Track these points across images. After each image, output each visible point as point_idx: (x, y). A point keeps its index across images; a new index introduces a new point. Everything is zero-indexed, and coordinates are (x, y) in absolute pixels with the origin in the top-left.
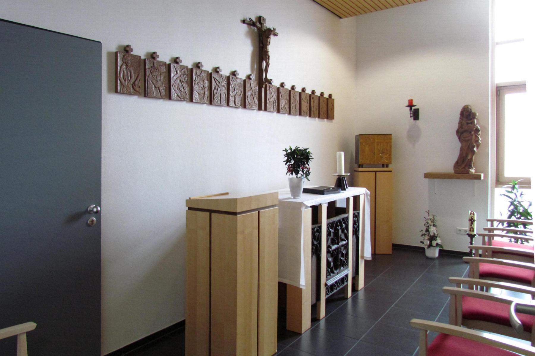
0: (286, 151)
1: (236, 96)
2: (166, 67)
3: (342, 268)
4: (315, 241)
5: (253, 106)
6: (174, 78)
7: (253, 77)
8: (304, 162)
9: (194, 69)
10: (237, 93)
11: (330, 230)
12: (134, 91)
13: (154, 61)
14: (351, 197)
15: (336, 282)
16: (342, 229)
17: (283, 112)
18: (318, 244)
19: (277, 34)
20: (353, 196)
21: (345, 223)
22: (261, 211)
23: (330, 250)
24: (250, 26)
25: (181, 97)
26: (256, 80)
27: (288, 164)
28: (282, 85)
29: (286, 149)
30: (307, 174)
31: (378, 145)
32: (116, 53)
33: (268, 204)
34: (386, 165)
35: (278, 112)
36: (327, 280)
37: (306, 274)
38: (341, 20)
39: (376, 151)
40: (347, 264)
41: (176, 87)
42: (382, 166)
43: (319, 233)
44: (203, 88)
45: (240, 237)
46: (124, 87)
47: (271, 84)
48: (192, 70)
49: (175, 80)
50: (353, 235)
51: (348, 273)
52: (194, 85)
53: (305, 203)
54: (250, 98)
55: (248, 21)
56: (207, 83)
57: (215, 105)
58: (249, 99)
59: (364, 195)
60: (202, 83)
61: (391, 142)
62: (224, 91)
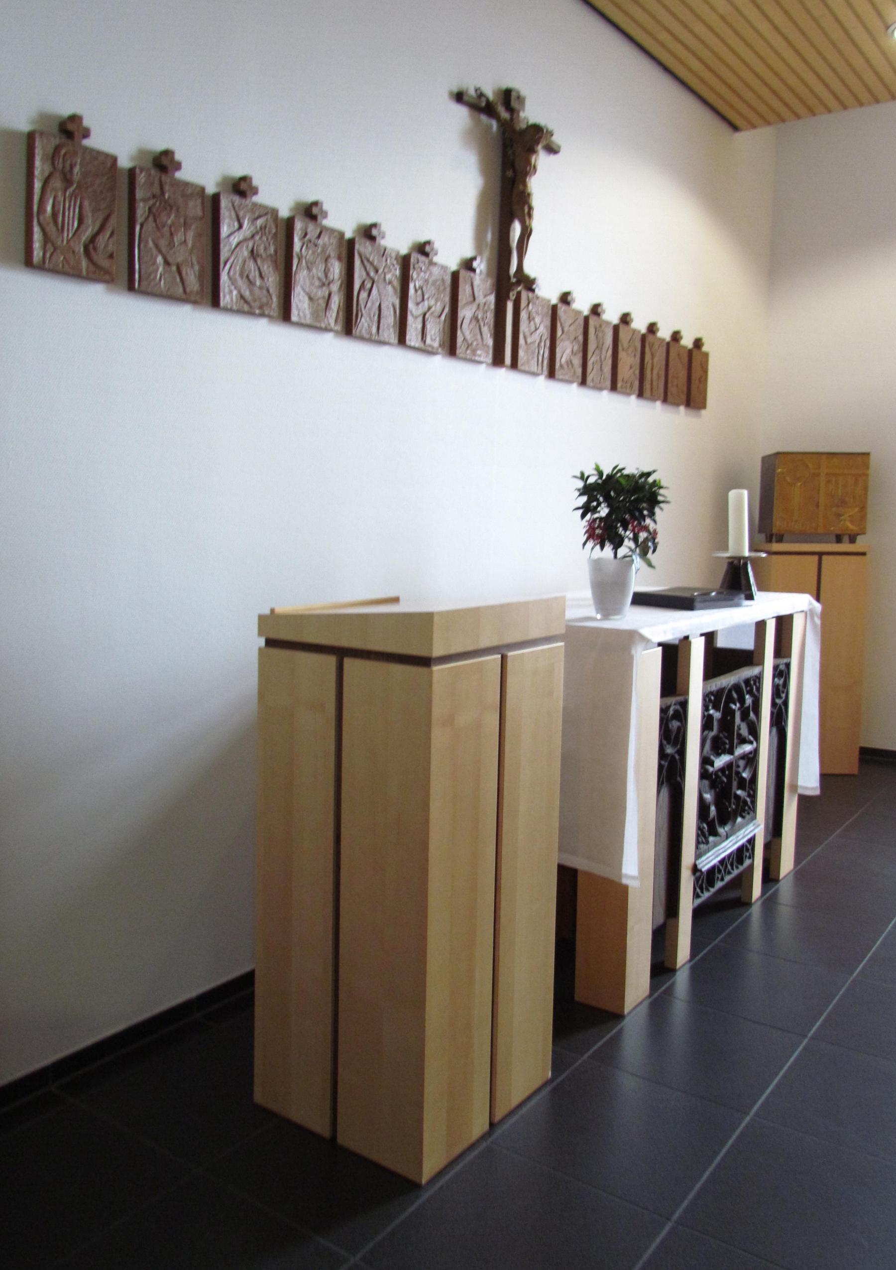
0: (582, 477)
1: (427, 316)
2: (203, 203)
3: (739, 820)
4: (668, 746)
5: (479, 352)
6: (232, 238)
7: (480, 265)
8: (641, 512)
9: (296, 220)
10: (429, 308)
11: (712, 712)
12: (92, 268)
13: (164, 178)
14: (769, 619)
15: (722, 862)
16: (742, 709)
17: (567, 377)
18: (676, 752)
19: (555, 148)
20: (776, 615)
21: (750, 692)
22: (510, 654)
23: (711, 769)
24: (476, 113)
25: (253, 304)
26: (488, 274)
27: (588, 516)
28: (565, 298)
29: (582, 474)
30: (644, 549)
31: (829, 482)
32: (31, 137)
33: (533, 634)
34: (850, 536)
35: (552, 374)
36: (698, 856)
37: (641, 841)
38: (738, 136)
39: (823, 500)
40: (753, 807)
41: (235, 269)
42: (834, 539)
43: (680, 720)
44: (325, 283)
45: (439, 737)
46: (55, 249)
47: (533, 291)
48: (289, 224)
49: (233, 247)
50: (771, 725)
51: (754, 836)
52: (294, 268)
53: (645, 632)
54: (471, 326)
55: (471, 97)
56: (336, 269)
57: (361, 338)
58: (465, 332)
59: (803, 614)
60: (322, 267)
61: (867, 475)
62: (391, 299)
